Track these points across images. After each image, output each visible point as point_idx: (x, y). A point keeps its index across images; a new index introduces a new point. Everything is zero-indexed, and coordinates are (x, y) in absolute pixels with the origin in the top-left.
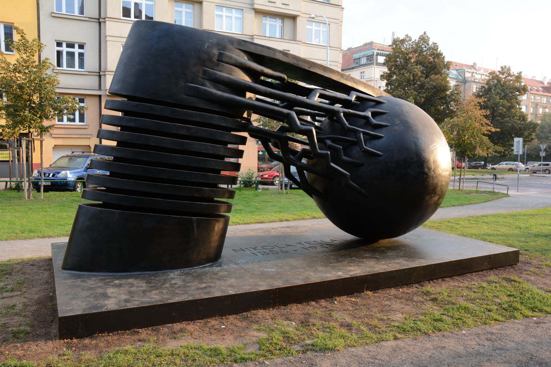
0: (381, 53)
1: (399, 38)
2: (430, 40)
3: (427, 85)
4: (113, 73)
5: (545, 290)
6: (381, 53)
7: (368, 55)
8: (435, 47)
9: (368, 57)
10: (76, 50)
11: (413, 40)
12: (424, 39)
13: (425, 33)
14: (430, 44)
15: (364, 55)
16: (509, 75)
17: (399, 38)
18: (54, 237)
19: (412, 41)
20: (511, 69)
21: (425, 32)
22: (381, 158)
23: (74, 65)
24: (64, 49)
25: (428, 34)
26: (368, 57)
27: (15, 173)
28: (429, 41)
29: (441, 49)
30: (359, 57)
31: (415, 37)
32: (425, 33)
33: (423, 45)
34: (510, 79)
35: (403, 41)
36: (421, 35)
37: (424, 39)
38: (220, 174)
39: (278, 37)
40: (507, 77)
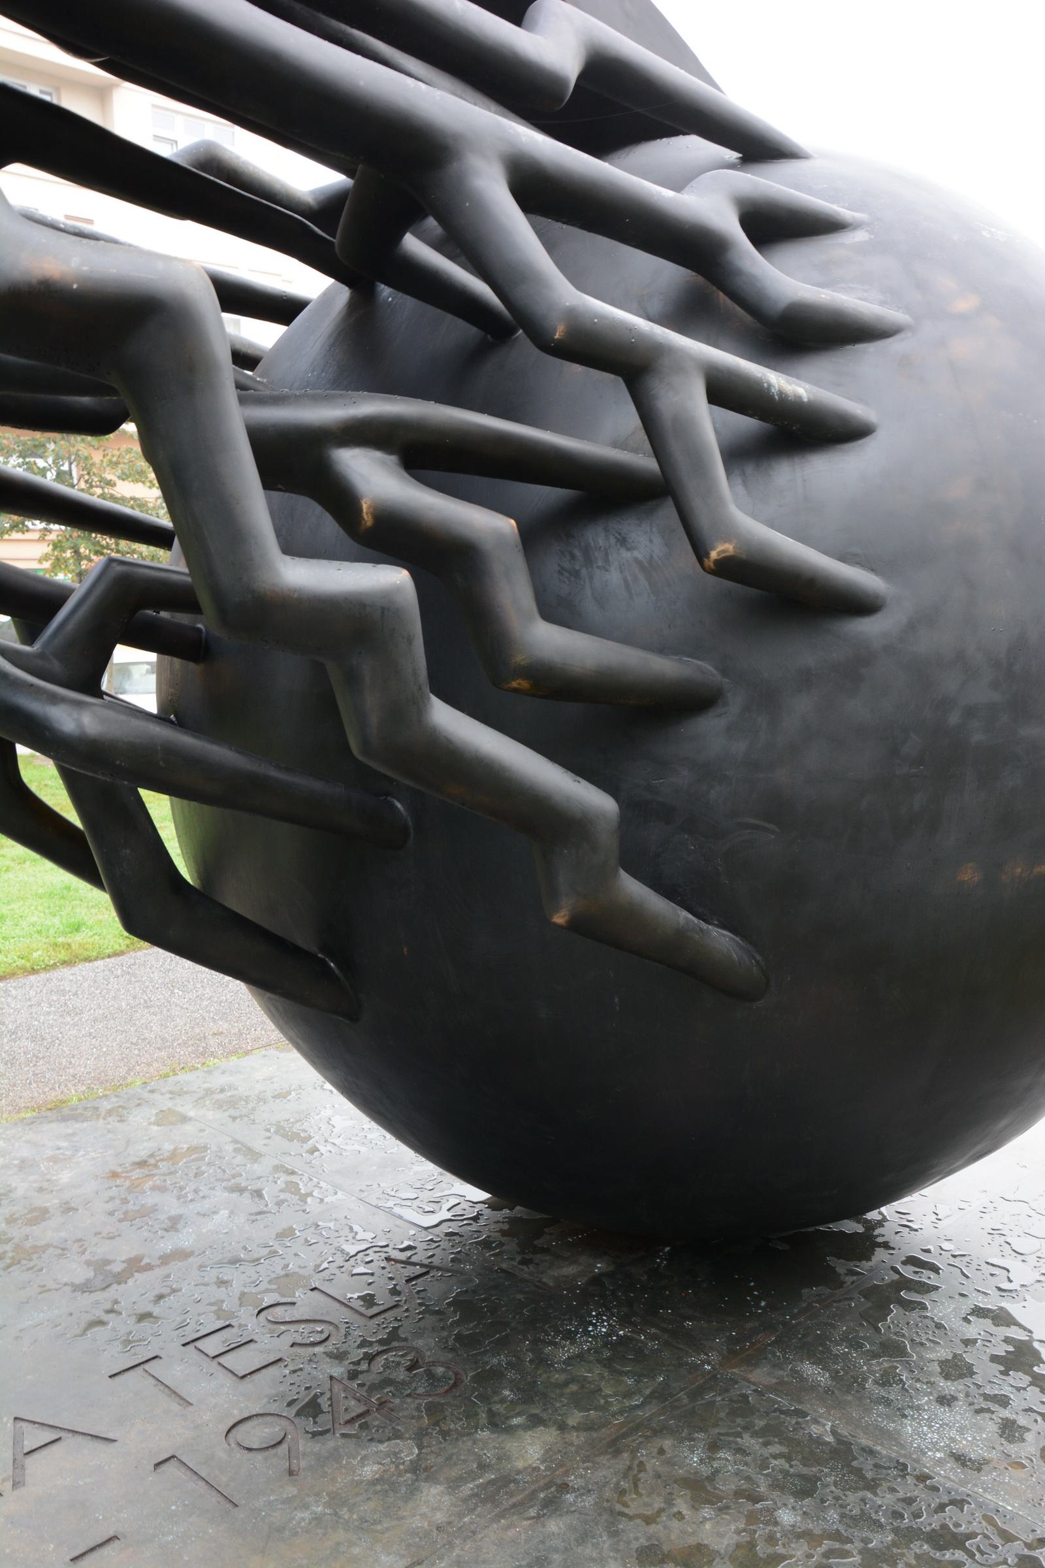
22: (867, 627)
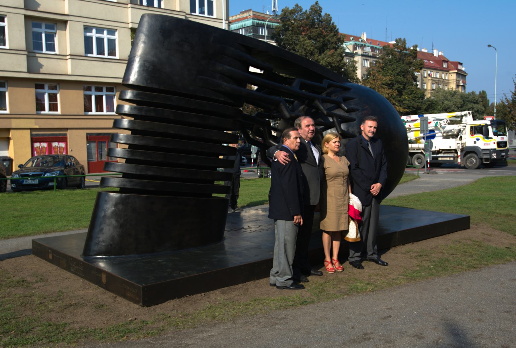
0: (261, 23)
1: (288, 8)
2: (322, 11)
3: (321, 61)
4: (127, 62)
5: (36, 289)
6: (261, 23)
7: (247, 26)
8: (328, 19)
9: (247, 29)
10: (105, 36)
11: (304, 10)
12: (316, 10)
13: (317, 3)
14: (323, 16)
15: (242, 25)
16: (405, 49)
17: (288, 8)
18: (313, 302)
19: (302, 12)
20: (406, 43)
21: (317, 2)
23: (104, 51)
24: (94, 34)
25: (320, 4)
26: (247, 29)
27: (32, 193)
28: (321, 12)
29: (335, 21)
30: (236, 28)
31: (306, 7)
32: (317, 3)
33: (315, 16)
34: (405, 53)
35: (293, 12)
36: (312, 4)
37: (316, 10)
38: (214, 184)
39: (179, 10)
40: (402, 50)
